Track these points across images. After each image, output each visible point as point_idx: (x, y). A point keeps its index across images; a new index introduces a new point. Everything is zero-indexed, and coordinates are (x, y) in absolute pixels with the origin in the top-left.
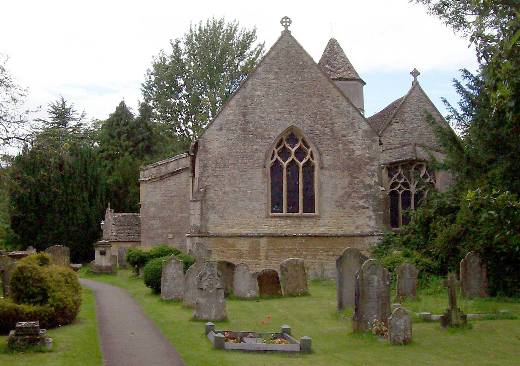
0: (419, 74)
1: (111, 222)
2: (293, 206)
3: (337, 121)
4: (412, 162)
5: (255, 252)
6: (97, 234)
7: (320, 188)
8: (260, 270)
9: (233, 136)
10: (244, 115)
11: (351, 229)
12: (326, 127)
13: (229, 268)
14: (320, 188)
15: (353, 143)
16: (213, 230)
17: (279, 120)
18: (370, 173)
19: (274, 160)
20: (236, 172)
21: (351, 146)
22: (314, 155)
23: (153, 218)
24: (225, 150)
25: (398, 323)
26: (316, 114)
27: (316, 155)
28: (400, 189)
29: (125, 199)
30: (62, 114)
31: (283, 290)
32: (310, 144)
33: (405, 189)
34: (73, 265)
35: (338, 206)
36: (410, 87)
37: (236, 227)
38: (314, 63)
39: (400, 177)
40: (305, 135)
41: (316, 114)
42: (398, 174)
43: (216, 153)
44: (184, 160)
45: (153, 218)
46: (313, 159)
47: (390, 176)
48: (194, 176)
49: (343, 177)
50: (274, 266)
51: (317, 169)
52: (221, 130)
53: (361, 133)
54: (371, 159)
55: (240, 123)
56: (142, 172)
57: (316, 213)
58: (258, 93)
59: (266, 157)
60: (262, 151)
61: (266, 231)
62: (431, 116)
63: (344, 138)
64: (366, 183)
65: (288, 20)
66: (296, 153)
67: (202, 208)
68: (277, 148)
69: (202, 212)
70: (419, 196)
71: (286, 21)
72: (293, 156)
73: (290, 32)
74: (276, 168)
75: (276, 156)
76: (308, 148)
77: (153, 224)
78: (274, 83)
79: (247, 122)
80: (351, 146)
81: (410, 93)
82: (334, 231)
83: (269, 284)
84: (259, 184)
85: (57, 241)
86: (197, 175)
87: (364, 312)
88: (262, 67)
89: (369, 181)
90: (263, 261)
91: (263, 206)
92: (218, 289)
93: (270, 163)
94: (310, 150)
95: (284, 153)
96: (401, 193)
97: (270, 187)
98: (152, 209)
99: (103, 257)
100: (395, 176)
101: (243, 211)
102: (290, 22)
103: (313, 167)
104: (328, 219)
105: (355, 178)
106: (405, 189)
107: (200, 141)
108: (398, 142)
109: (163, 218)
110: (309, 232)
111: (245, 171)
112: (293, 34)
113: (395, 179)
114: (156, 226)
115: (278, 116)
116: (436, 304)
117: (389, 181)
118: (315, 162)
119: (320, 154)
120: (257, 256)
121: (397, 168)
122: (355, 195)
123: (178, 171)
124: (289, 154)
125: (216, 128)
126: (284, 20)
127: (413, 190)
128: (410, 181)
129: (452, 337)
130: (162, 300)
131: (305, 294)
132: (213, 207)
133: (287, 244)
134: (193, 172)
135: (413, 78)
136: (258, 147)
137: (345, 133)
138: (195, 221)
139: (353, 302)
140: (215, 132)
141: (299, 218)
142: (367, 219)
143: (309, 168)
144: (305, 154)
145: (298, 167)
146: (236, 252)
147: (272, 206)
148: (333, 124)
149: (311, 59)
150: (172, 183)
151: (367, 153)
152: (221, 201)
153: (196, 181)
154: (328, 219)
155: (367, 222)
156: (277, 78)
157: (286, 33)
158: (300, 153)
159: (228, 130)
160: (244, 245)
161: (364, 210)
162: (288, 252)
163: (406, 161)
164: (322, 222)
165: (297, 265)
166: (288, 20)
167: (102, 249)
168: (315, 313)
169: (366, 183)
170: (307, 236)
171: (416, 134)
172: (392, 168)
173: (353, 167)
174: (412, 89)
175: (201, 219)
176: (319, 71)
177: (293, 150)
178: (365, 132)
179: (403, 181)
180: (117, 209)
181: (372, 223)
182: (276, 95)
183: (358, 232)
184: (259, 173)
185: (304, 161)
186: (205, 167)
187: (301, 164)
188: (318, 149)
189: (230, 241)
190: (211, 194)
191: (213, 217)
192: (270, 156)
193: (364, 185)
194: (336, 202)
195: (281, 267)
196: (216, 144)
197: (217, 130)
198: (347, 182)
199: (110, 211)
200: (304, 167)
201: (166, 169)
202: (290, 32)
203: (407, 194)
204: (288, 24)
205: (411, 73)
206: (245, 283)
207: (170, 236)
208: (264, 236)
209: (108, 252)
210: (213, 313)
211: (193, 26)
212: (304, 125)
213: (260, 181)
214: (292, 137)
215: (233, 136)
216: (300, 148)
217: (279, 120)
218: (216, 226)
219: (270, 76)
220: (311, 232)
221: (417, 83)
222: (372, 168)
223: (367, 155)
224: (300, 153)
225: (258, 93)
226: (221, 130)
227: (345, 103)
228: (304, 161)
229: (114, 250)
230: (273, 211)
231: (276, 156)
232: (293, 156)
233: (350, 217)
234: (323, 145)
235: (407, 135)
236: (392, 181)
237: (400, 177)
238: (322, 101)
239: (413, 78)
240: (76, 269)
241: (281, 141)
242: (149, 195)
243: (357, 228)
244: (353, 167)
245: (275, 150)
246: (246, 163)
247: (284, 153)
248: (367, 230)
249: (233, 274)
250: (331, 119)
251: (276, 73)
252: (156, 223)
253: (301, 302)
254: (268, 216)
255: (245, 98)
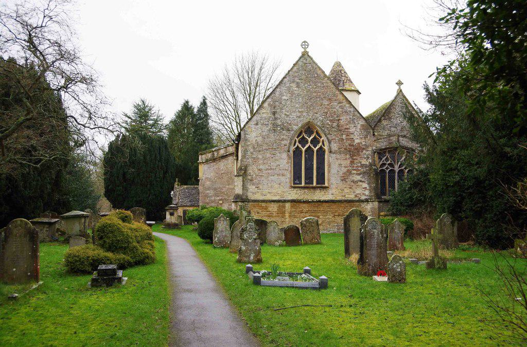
0: (403, 84)
1: (178, 193)
2: (309, 179)
3: (342, 118)
4: (396, 149)
5: (282, 212)
6: (169, 200)
7: (329, 166)
8: (285, 226)
9: (266, 129)
10: (274, 113)
11: (351, 197)
12: (334, 122)
13: (261, 225)
14: (329, 166)
15: (353, 134)
16: (251, 197)
17: (299, 117)
18: (365, 156)
19: (296, 146)
20: (268, 155)
21: (352, 136)
22: (325, 143)
23: (209, 189)
24: (260, 139)
25: (395, 266)
26: (327, 113)
27: (326, 143)
28: (387, 168)
29: (190, 177)
30: (143, 112)
31: (303, 241)
32: (322, 135)
33: (391, 168)
34: (148, 222)
35: (342, 180)
36: (395, 94)
37: (268, 195)
38: (325, 76)
39: (387, 159)
40: (318, 128)
41: (327, 113)
42: (385, 157)
43: (254, 141)
44: (230, 148)
45: (209, 189)
46: (324, 146)
47: (380, 159)
48: (237, 159)
49: (346, 159)
50: (296, 223)
51: (327, 152)
52: (257, 124)
53: (359, 127)
54: (367, 147)
55: (271, 119)
56: (200, 156)
57: (326, 185)
58: (284, 98)
59: (290, 144)
60: (287, 139)
61: (290, 198)
62: (411, 114)
63: (346, 130)
64: (362, 163)
65: (306, 44)
66: (312, 141)
67: (243, 181)
68: (298, 137)
69: (243, 184)
70: (401, 172)
71: (305, 44)
72: (309, 144)
73: (308, 52)
74: (297, 152)
75: (297, 143)
76: (321, 137)
77: (208, 193)
78: (295, 90)
79: (276, 119)
80: (352, 136)
81: (396, 98)
82: (339, 198)
83: (293, 237)
84: (284, 162)
85: (139, 204)
86: (240, 159)
87: (370, 256)
88: (288, 78)
89: (364, 162)
90: (287, 220)
91: (288, 180)
92: (255, 239)
93: (293, 148)
94: (322, 139)
95: (303, 141)
96: (387, 171)
97: (292, 166)
98: (208, 183)
99: (172, 217)
100: (384, 159)
101: (274, 183)
102: (308, 46)
103: (324, 151)
104: (335, 189)
105: (355, 159)
106: (391, 168)
107: (242, 133)
108: (386, 134)
109: (215, 189)
110: (320, 199)
111: (274, 154)
112: (310, 54)
113: (383, 161)
114: (210, 195)
115: (299, 114)
116: (423, 249)
117: (379, 162)
118: (326, 148)
119: (330, 142)
120: (283, 217)
121: (385, 152)
122: (355, 172)
123: (227, 155)
124: (307, 142)
125: (254, 123)
126: (304, 44)
127: (397, 168)
128: (395, 162)
129: (127, 272)
130: (215, 247)
131: (319, 243)
132: (251, 180)
133: (305, 207)
134: (237, 156)
135: (397, 87)
136: (285, 137)
137: (348, 127)
138: (239, 190)
139: (358, 249)
140: (253, 126)
141: (314, 188)
142: (363, 190)
143: (321, 152)
144: (319, 142)
145: (313, 151)
146: (269, 214)
147: (294, 180)
148: (339, 120)
149: (323, 72)
150: (222, 164)
151: (363, 142)
152: (257, 175)
153: (239, 161)
154: (335, 189)
155: (363, 189)
156: (298, 87)
157: (305, 55)
158: (315, 142)
159: (263, 124)
160: (274, 208)
161: (361, 183)
162: (305, 213)
163: (391, 148)
164: (330, 192)
165: (313, 223)
166: (304, 46)
167: (171, 211)
168: (327, 257)
169: (362, 163)
170: (320, 201)
171: (399, 128)
172: (381, 153)
173: (354, 151)
174: (398, 94)
175: (243, 189)
176: (328, 81)
177: (310, 140)
178: (362, 126)
179: (389, 162)
180: (184, 182)
181: (367, 193)
182: (297, 99)
183: (357, 199)
184: (285, 155)
185: (317, 147)
186: (245, 151)
187: (315, 149)
188: (328, 139)
189: (263, 204)
190: (250, 171)
191: (252, 188)
192: (293, 144)
193: (361, 165)
194: (341, 177)
195: (302, 224)
196: (254, 134)
197: (254, 124)
198: (349, 163)
199: (178, 185)
200: (317, 151)
201: (218, 154)
202: (308, 52)
203: (392, 171)
204: (306, 46)
205: (397, 84)
206: (274, 233)
207: (221, 202)
208: (288, 201)
209: (175, 214)
210: (252, 258)
211: (240, 72)
212: (318, 119)
213: (286, 161)
214: (309, 129)
215: (266, 129)
216: (315, 138)
217: (299, 117)
218: (254, 193)
219: (294, 85)
220: (323, 199)
221: (401, 91)
222: (367, 153)
223: (364, 143)
224: (315, 142)
225: (284, 98)
226: (257, 124)
227: (347, 105)
228: (317, 147)
229: (180, 212)
230: (294, 184)
231: (297, 143)
232: (309, 144)
233: (350, 188)
234: (331, 136)
235: (393, 129)
236: (381, 163)
237: (387, 159)
238: (331, 103)
239: (397, 87)
240: (150, 225)
241: (301, 133)
242: (205, 172)
243: (356, 196)
244: (354, 151)
245: (297, 139)
246: (275, 149)
247: (303, 141)
248: (363, 198)
249: (266, 228)
250: (337, 117)
251: (297, 83)
252: (211, 193)
253: (318, 247)
254: (292, 187)
255: (275, 101)
